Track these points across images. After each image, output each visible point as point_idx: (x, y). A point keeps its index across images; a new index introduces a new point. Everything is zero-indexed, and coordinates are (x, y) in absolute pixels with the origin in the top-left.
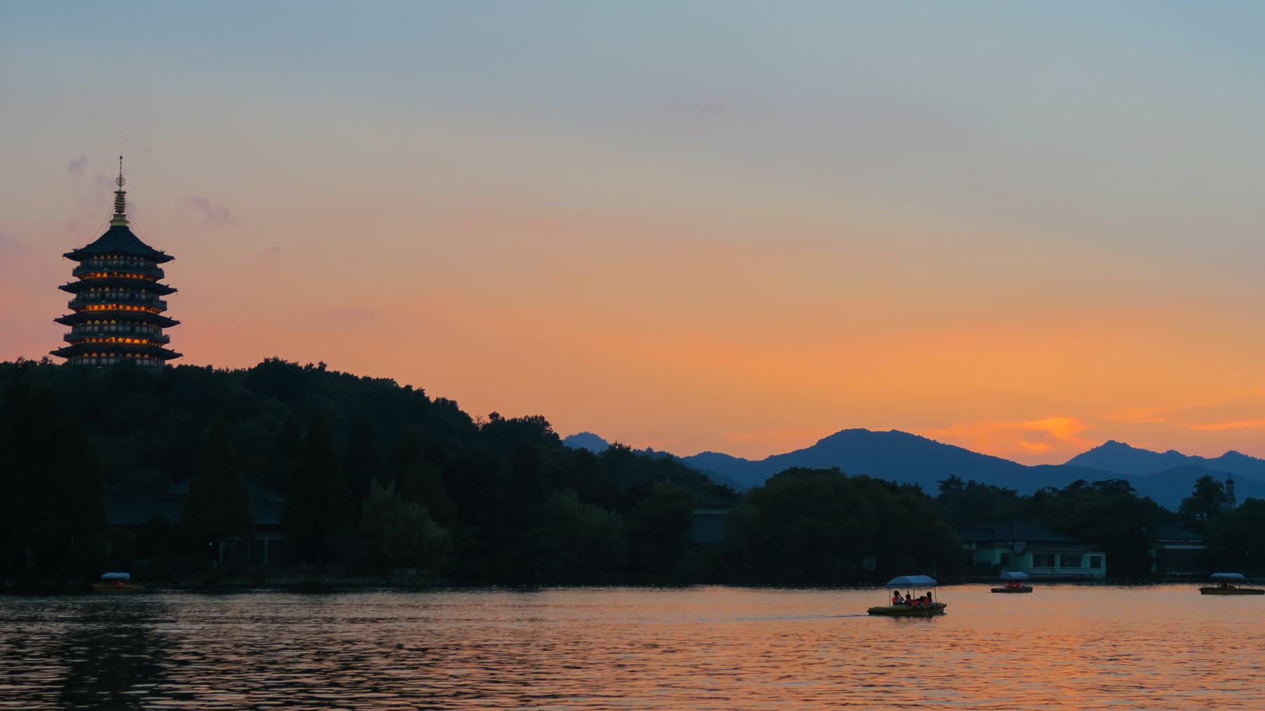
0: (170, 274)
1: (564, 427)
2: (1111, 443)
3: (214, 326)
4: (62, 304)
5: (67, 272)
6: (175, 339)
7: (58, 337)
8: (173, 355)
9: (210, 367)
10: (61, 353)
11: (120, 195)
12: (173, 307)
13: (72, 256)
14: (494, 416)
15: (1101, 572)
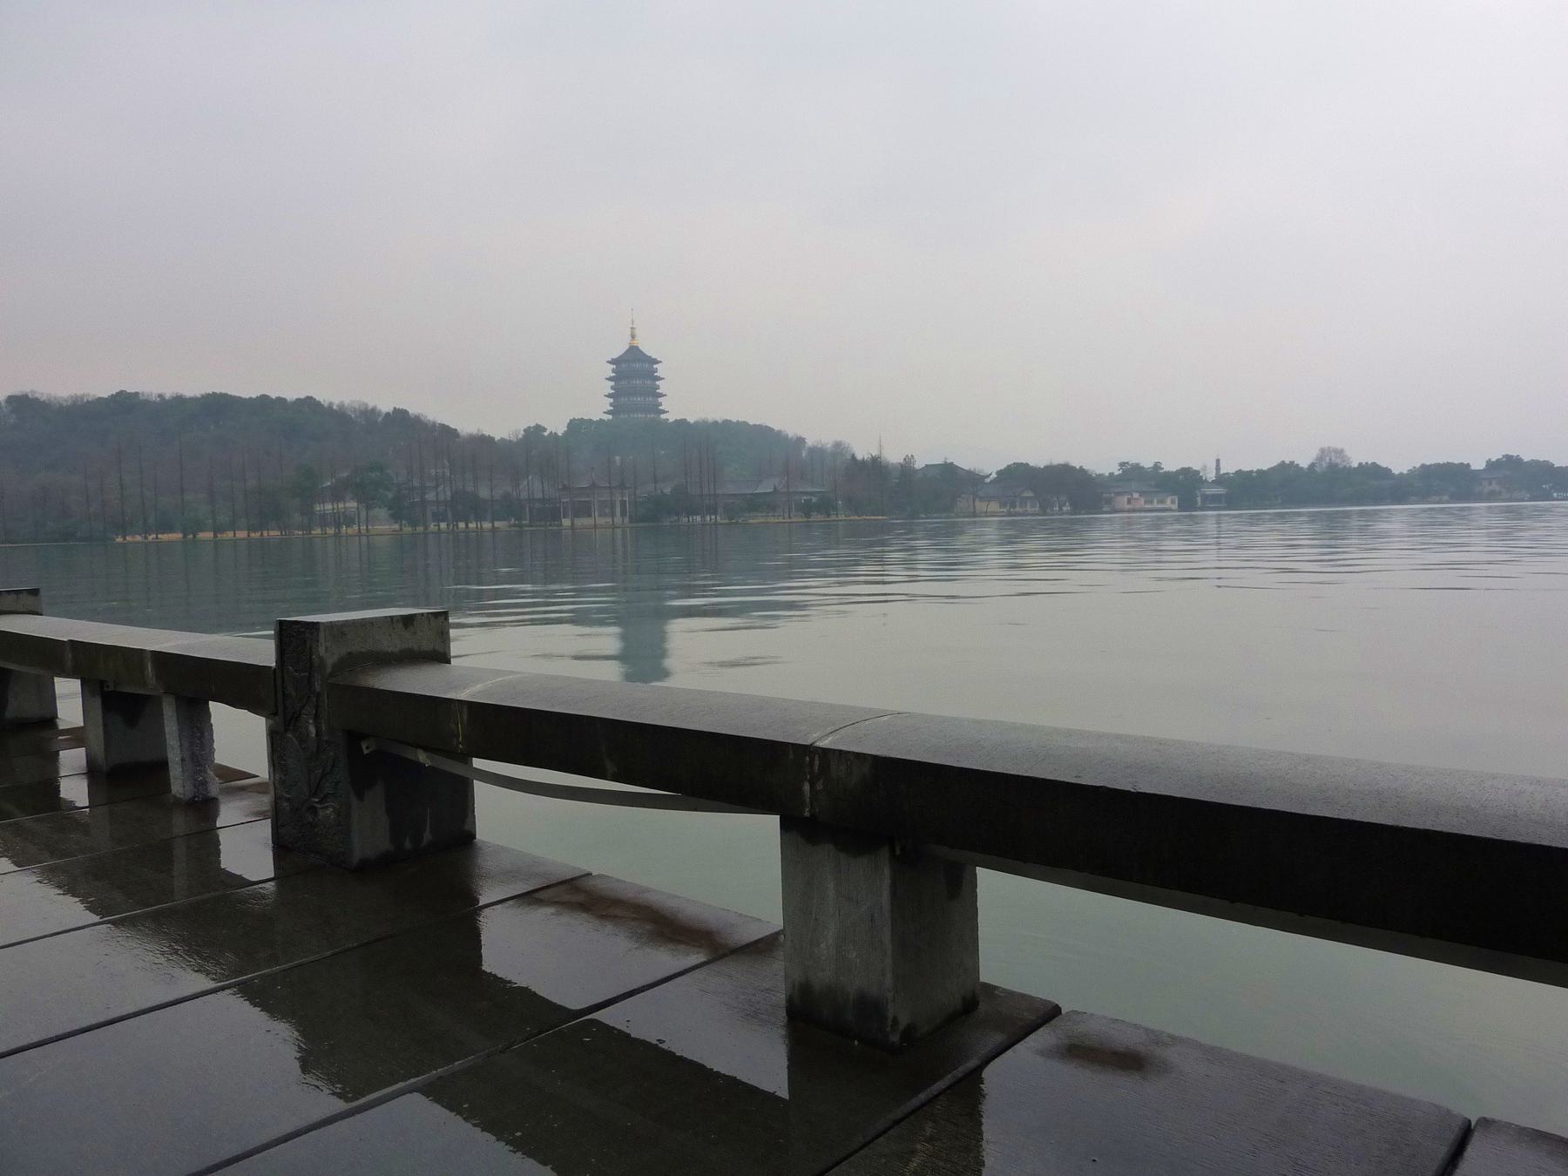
0: (661, 370)
1: (691, 420)
2: (310, 398)
3: (686, 399)
4: (608, 387)
5: (609, 370)
6: (665, 404)
7: (607, 404)
8: (664, 412)
9: (1157, 466)
10: (608, 412)
11: (576, 658)
12: (663, 387)
13: (612, 362)
14: (1122, 464)
15: (1175, 506)
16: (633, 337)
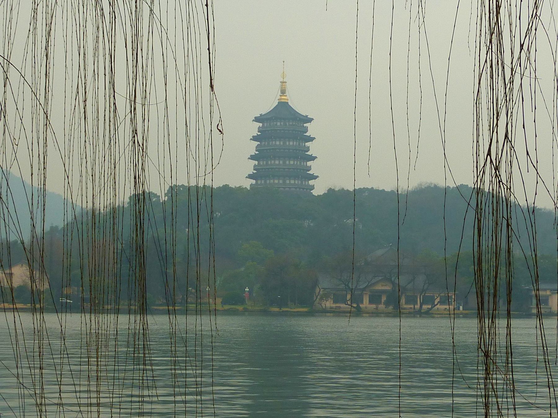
0: (312, 129)
3: (333, 169)
4: (252, 148)
5: (254, 129)
7: (250, 167)
12: (313, 148)
13: (257, 120)
16: (283, 92)
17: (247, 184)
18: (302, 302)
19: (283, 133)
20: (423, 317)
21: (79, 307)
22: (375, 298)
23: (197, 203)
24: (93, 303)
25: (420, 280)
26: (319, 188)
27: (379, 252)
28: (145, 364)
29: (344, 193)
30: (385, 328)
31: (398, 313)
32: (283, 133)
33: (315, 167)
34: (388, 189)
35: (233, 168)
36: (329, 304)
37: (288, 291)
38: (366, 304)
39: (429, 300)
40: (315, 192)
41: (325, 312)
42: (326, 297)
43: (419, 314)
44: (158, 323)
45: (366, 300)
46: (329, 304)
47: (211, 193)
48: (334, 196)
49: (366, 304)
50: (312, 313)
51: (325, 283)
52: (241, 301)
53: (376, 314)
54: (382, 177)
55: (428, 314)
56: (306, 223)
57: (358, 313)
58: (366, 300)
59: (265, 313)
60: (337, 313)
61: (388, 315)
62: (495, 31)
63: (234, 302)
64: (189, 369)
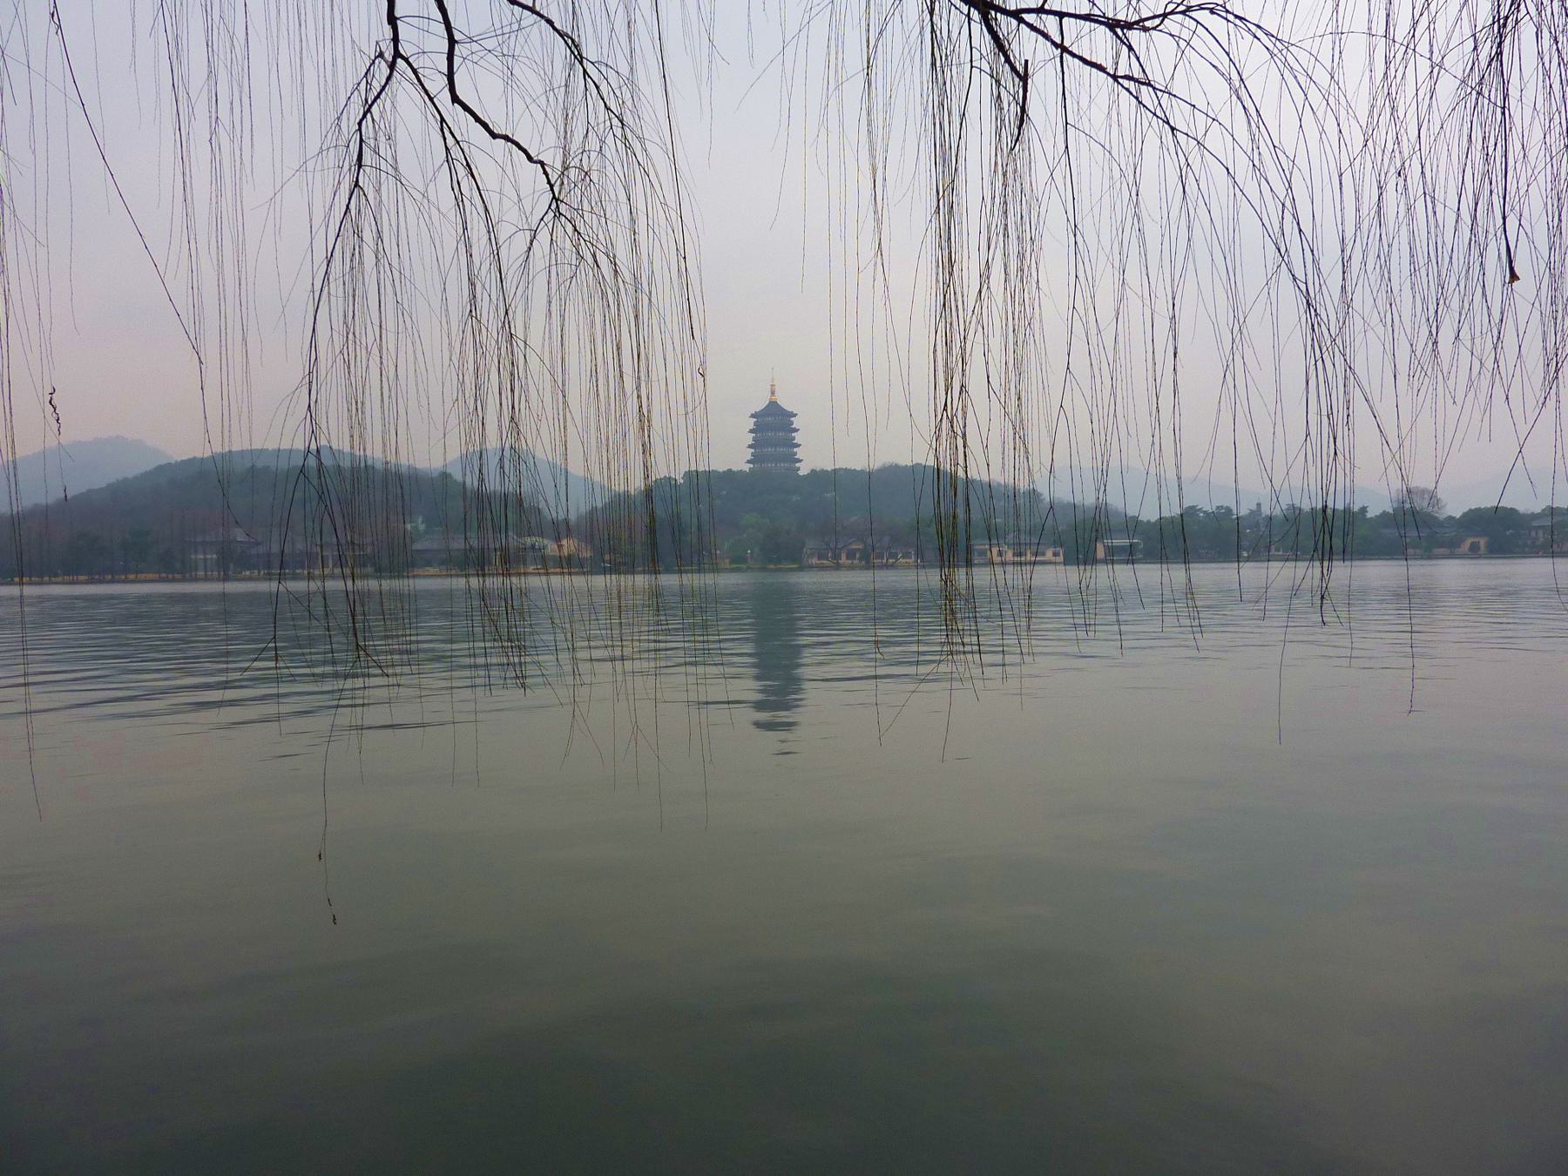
0: (796, 422)
4: (749, 438)
5: (751, 423)
7: (748, 454)
12: (798, 438)
13: (753, 416)
17: (747, 468)
18: (794, 561)
19: (774, 426)
20: (1437, 557)
21: (604, 572)
22: (851, 555)
23: (701, 484)
24: (621, 565)
25: (887, 539)
26: (804, 470)
27: (854, 519)
28: (510, 640)
29: (824, 472)
30: (861, 579)
31: (869, 566)
32: (774, 426)
33: (800, 453)
34: (858, 468)
35: (731, 451)
36: (814, 561)
37: (780, 551)
38: (843, 560)
39: (894, 556)
40: (801, 473)
41: (811, 567)
42: (812, 555)
43: (887, 566)
44: (669, 581)
45: (844, 556)
46: (814, 561)
47: (709, 474)
48: (820, 478)
49: (843, 560)
50: (801, 569)
51: (811, 544)
52: (744, 560)
53: (852, 568)
54: (854, 456)
55: (892, 566)
56: (795, 498)
57: (838, 567)
58: (844, 556)
59: (763, 569)
60: (822, 568)
61: (862, 568)
62: (949, 265)
63: (738, 562)
64: (596, 637)
